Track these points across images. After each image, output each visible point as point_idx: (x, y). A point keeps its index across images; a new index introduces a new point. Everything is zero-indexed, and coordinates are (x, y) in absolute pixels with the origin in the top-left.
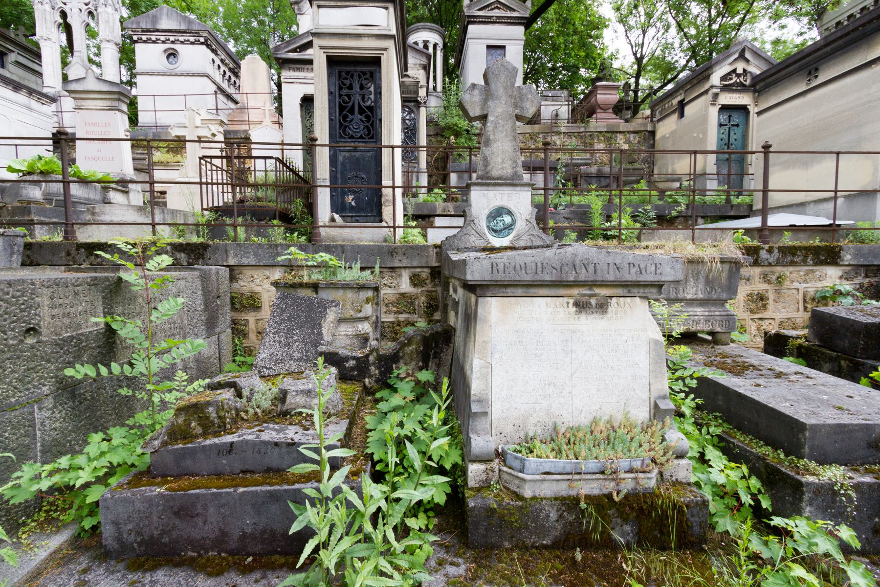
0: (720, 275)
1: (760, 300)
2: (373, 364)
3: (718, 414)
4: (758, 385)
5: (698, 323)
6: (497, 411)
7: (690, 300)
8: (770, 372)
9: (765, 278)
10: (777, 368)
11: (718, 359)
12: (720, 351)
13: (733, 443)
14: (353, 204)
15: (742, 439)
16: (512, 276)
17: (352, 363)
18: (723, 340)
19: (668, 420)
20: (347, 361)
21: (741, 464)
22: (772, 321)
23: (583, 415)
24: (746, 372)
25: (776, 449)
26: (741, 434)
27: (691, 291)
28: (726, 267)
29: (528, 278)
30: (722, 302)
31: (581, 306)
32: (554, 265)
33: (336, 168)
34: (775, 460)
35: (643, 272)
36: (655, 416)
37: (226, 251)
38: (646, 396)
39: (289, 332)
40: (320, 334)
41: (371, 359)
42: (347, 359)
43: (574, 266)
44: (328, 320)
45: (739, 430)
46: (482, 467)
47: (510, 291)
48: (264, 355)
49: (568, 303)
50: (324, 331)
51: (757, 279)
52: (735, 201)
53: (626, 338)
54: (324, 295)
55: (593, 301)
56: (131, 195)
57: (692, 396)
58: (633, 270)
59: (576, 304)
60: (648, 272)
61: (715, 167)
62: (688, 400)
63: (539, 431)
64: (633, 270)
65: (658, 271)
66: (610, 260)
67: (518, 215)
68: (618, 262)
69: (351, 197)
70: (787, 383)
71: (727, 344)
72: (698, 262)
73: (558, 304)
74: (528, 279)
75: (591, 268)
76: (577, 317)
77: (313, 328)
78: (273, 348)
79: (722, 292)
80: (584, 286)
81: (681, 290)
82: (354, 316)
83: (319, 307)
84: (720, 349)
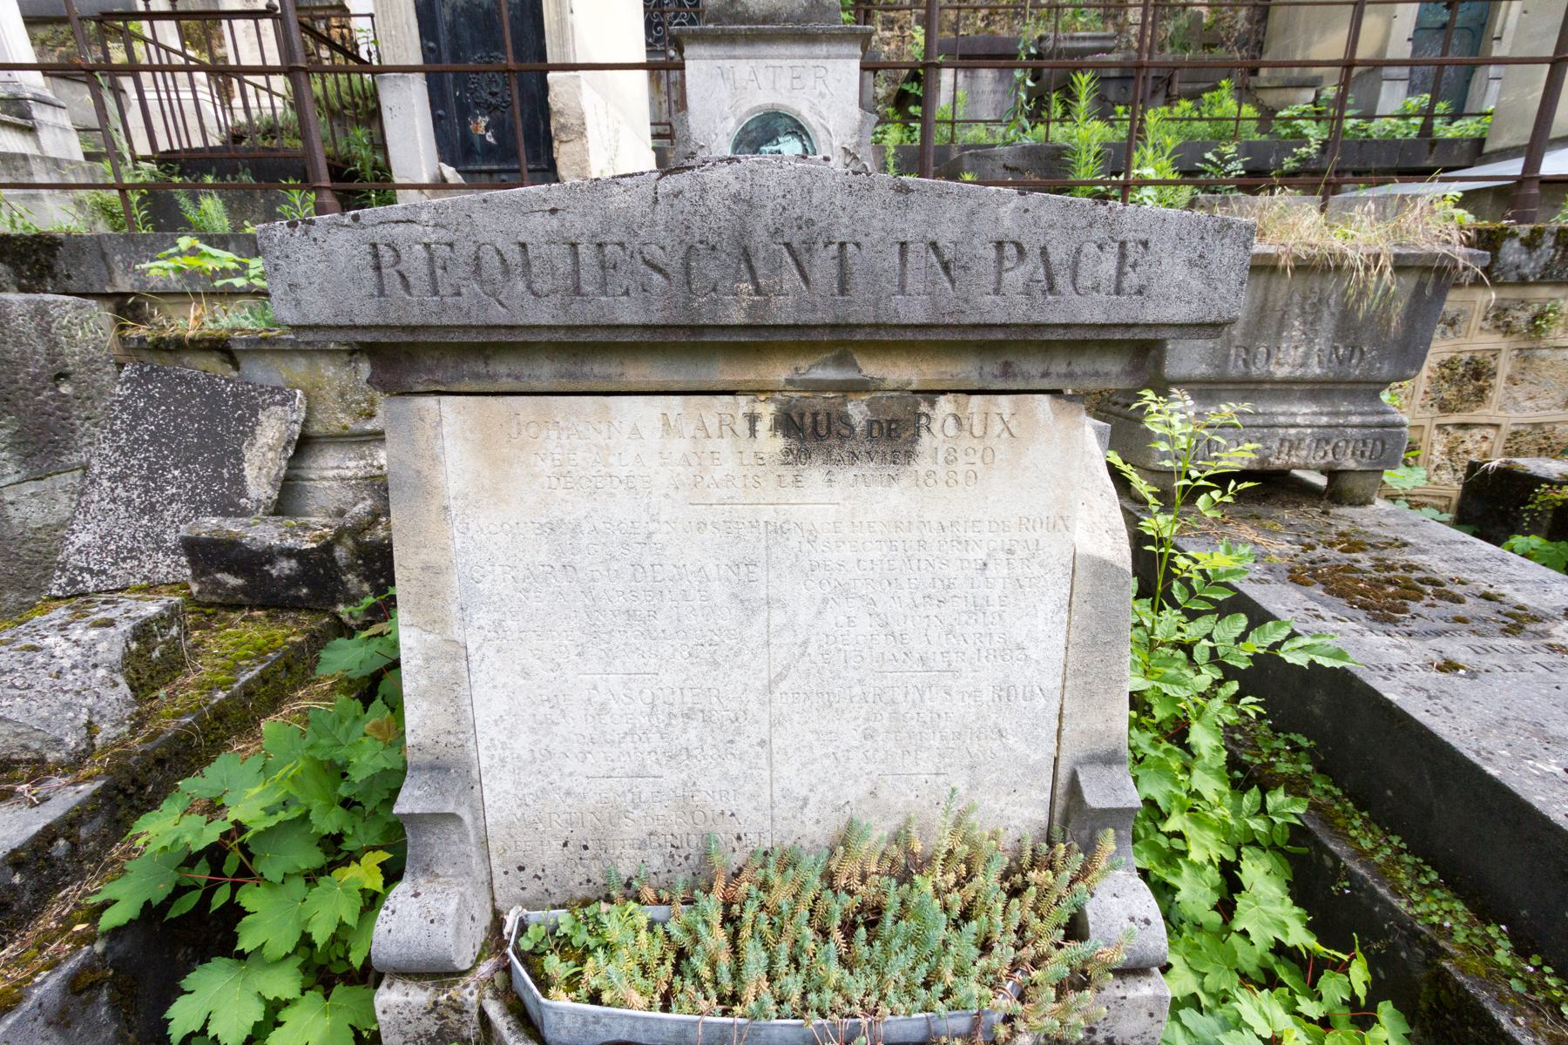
0: (1386, 309)
1: (1473, 377)
2: (350, 567)
3: (1303, 741)
4: (1449, 666)
5: (1294, 445)
6: (501, 796)
7: (1285, 381)
8: (1486, 609)
9: (1500, 320)
10: (1507, 589)
11: (1334, 554)
12: (1343, 527)
13: (1336, 859)
14: (490, 138)
15: (1367, 844)
16: (472, 306)
17: (286, 566)
18: (1358, 491)
19: (1108, 842)
20: (271, 561)
21: (1348, 949)
22: (1490, 432)
23: (811, 812)
24: (1414, 607)
25: (1484, 913)
26: (1366, 822)
27: (1292, 357)
28: (1410, 282)
29: (543, 314)
30: (1370, 388)
31: (809, 431)
32: (659, 256)
33: (436, 40)
34: (1475, 963)
35: (1062, 281)
36: (1066, 821)
37: (104, 256)
38: (1041, 755)
39: (153, 475)
40: (238, 480)
41: (341, 553)
42: (270, 555)
43: (747, 256)
44: (261, 440)
45: (1360, 807)
46: (420, 996)
47: (503, 370)
48: (84, 538)
49: (753, 419)
50: (250, 472)
51: (1477, 320)
52: (1444, 130)
53: (981, 555)
54: (259, 371)
55: (858, 411)
56: (45, 136)
57: (1234, 686)
58: (1016, 276)
59: (788, 423)
60: (1085, 281)
61: (1409, 47)
62: (1217, 704)
63: (657, 862)
64: (1016, 276)
65: (1132, 279)
66: (911, 226)
67: (822, 135)
68: (946, 235)
69: (483, 121)
70: (1542, 657)
71: (1366, 502)
72: (1326, 270)
73: (712, 423)
74: (545, 319)
75: (823, 266)
76: (788, 473)
77: (220, 463)
78: (111, 519)
79: (1381, 358)
80: (812, 348)
81: (1262, 356)
82: (355, 427)
83: (237, 406)
84: (1346, 517)
